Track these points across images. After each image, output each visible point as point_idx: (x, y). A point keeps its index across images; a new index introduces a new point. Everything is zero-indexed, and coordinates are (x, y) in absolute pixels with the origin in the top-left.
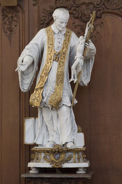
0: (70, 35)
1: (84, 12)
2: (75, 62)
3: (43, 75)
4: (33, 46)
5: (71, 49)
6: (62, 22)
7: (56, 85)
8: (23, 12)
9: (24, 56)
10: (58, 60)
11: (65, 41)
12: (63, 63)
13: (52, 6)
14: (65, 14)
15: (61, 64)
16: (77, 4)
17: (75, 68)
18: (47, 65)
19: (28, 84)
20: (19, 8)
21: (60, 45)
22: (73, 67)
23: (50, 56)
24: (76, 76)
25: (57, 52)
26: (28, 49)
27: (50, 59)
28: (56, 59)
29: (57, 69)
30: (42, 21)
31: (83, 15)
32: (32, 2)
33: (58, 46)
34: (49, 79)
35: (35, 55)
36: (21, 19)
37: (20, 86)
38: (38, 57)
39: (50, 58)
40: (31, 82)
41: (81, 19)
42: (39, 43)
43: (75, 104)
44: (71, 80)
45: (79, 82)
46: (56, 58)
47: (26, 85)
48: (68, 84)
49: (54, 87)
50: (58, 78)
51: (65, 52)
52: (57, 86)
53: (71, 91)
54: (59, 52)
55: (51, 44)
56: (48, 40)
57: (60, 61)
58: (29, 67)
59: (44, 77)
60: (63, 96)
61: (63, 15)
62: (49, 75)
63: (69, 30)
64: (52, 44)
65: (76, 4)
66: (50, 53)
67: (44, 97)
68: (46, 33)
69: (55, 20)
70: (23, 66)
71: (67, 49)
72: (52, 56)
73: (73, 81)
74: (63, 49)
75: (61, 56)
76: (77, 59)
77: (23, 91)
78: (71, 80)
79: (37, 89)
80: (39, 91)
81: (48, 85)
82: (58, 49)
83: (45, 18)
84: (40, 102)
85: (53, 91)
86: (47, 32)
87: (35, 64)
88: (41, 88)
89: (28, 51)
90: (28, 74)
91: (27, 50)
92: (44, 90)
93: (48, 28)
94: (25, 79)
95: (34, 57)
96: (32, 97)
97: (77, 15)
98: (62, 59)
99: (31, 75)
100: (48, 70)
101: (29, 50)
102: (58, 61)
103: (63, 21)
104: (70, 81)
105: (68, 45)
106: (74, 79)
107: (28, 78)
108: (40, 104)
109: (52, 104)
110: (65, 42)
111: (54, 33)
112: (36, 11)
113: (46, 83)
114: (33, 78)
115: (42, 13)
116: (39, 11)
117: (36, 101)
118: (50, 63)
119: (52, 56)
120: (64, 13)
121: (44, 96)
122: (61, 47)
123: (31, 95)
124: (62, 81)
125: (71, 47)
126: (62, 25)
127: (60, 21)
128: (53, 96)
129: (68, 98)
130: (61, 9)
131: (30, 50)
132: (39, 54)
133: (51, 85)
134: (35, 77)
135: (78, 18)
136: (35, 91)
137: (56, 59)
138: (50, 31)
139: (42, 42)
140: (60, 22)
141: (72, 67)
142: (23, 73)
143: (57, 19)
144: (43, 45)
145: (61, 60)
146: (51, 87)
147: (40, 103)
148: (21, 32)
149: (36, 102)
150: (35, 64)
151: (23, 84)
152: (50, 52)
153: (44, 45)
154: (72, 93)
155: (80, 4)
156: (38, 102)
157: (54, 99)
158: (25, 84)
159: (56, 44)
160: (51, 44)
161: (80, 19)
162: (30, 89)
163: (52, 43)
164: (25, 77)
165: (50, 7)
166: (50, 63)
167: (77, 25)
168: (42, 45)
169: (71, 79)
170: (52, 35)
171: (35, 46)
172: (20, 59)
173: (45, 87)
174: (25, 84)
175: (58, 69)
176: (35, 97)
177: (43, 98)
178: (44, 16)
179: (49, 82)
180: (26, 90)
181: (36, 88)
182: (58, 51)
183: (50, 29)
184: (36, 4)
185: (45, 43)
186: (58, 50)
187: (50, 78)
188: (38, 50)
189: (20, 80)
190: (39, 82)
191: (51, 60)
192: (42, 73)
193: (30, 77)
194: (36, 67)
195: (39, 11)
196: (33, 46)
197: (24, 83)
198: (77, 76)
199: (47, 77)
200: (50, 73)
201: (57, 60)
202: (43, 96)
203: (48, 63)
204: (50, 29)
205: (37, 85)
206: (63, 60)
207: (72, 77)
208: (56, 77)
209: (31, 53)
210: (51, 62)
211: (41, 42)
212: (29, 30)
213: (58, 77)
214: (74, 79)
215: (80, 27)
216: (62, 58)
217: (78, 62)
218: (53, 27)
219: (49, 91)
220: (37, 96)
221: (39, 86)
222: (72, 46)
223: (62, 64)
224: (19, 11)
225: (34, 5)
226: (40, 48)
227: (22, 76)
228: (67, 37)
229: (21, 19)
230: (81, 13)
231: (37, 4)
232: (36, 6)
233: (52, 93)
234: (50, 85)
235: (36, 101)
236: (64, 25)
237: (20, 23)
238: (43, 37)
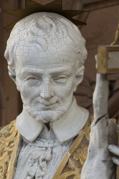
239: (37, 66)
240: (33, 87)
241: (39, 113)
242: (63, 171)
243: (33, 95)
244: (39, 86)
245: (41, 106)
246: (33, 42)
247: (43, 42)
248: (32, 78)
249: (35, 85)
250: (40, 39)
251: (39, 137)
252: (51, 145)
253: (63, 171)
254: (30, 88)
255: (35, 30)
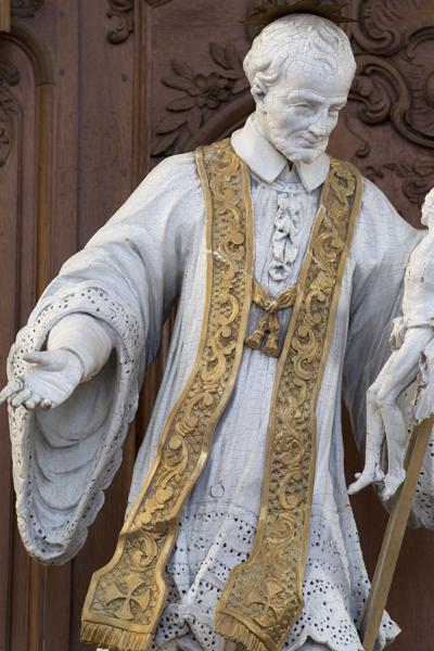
0: (351, 198)
1: (426, 85)
2: (395, 357)
3: (175, 443)
4: (112, 263)
5: (360, 286)
6: (312, 105)
7: (264, 511)
8: (43, 80)
9: (50, 316)
10: (280, 343)
11: (322, 227)
12: (307, 364)
13: (225, 51)
14: (329, 49)
15: (298, 368)
16: (386, 35)
17: (391, 398)
18: (205, 375)
19: (72, 508)
20: (18, 57)
21: (292, 254)
22: (381, 386)
23: (224, 321)
24: (397, 453)
25: (272, 298)
26: (77, 276)
27: (226, 341)
28: (264, 339)
29: (267, 404)
30: (161, 135)
31: (418, 104)
32: (102, 23)
33: (278, 253)
34: (214, 470)
35: (129, 311)
36: (29, 127)
37: (20, 522)
38: (142, 333)
39: (226, 332)
40: (93, 498)
41: (408, 125)
42: (154, 237)
43: (383, 644)
44: (363, 479)
45: (413, 504)
46: (267, 332)
47: (59, 518)
48: (339, 511)
49: (251, 520)
50: (276, 462)
51: (322, 297)
52: (271, 519)
53: (360, 554)
54: (283, 298)
55: (235, 247)
56: (214, 218)
57: (289, 355)
58: (82, 388)
59: (185, 452)
60: (309, 588)
61: (318, 54)
62: (217, 446)
63: (347, 169)
64: (237, 246)
65: (374, 33)
66: (227, 303)
67: (180, 589)
68: (198, 177)
69: (262, 95)
70: (49, 376)
71: (338, 280)
72: (239, 317)
73: (372, 490)
74: (311, 274)
75: (299, 322)
76: (411, 333)
77: (38, 553)
78: (363, 479)
79: (133, 537)
80: (149, 548)
81: (209, 508)
82: (278, 276)
83: (179, 119)
84: (154, 618)
85: (245, 548)
86: (207, 172)
87: (126, 372)
88: (165, 529)
89: (78, 288)
90: (74, 444)
91: (70, 283)
92: (181, 544)
93: (212, 151)
94: (51, 476)
95: (121, 324)
96: (102, 587)
97: (385, 102)
98: (305, 340)
99: (97, 456)
100: (211, 407)
101: (84, 285)
102: (278, 356)
103: (315, 96)
104: (356, 487)
105: (340, 254)
106: (380, 475)
107: (76, 471)
108: (155, 633)
109: (236, 632)
110: (324, 236)
111: (255, 180)
112: (124, 78)
113: (197, 497)
114: (106, 468)
115: (167, 90)
116: (141, 77)
117: (125, 611)
118: (222, 364)
119: (239, 317)
120: (323, 44)
121: (181, 580)
122: (297, 266)
123: (96, 575)
124: (302, 486)
125: (357, 273)
126: (304, 121)
127: (294, 93)
128: (246, 580)
129: (340, 598)
130: (302, 19)
131: (91, 283)
132: (152, 315)
133: (232, 509)
134: (119, 460)
135: (388, 120)
136: (119, 551)
137: (264, 339)
138: (223, 165)
139: (172, 238)
140: (293, 101)
141: (373, 387)
142: (38, 413)
143: (275, 81)
144: (178, 252)
145: (296, 343)
146: (228, 522)
147: (149, 628)
148: (29, 202)
149: (125, 624)
150: (126, 372)
151: (41, 508)
152: (224, 296)
153: (188, 253)
154: (364, 572)
155: (403, 35)
156: (140, 621)
157: (253, 597)
158: (53, 509)
159: (266, 247)
160: (235, 247)
161: (402, 127)
162: (83, 539)
163: (238, 240)
164: (51, 464)
165: (211, 52)
166: (222, 364)
167: (385, 166)
168: (172, 251)
169: (361, 470)
170: (236, 192)
171: (129, 260)
172: (28, 338)
173: (186, 524)
174: (53, 509)
175: (278, 402)
176: (121, 586)
177: (174, 595)
178: (174, 108)
179: (216, 491)
180: (60, 546)
181: (125, 529)
182: (277, 290)
183: (221, 157)
184: (123, 34)
185: (190, 245)
186: (279, 281)
187: (221, 461)
188: (143, 287)
189: (19, 482)
190: (150, 491)
191: (233, 345)
192: (171, 432)
193: (90, 462)
194: (130, 392)
195: (141, 77)
196: (113, 257)
197: (44, 502)
198: (402, 454)
199: (204, 456)
200: (225, 429)
201: (272, 342)
202: (172, 585)
203: (213, 364)
204: (221, 157)
205: (130, 511)
206: (313, 345)
207: (371, 457)
208: (261, 457)
209: (100, 302)
210: (230, 358)
211: (165, 237)
212: (79, 190)
213: (275, 457)
214: (380, 475)
215: (400, 175)
216: (302, 331)
217: (415, 355)
218: (245, 141)
219: (214, 551)
220: (133, 580)
221: (145, 518)
222: (366, 271)
223: (306, 374)
224: (17, 73)
225: (114, 41)
226: (159, 273)
227: (32, 457)
228: (339, 212)
229: (29, 127)
230: (410, 91)
231: (131, 32)
232: (122, 48)
233: (233, 562)
234: (220, 507)
235: (125, 611)
236: (323, 123)
237: (21, 144)
238: (180, 202)
239: (320, 92)
240: (301, 117)
241: (298, 150)
242: (319, 232)
243: (297, 126)
244: (309, 116)
245: (302, 142)
246: (320, 60)
247: (334, 64)
248: (304, 106)
249: (304, 114)
250: (329, 58)
251: (277, 180)
252: (294, 191)
253: (319, 232)
254: (295, 117)
255: (319, 41)
